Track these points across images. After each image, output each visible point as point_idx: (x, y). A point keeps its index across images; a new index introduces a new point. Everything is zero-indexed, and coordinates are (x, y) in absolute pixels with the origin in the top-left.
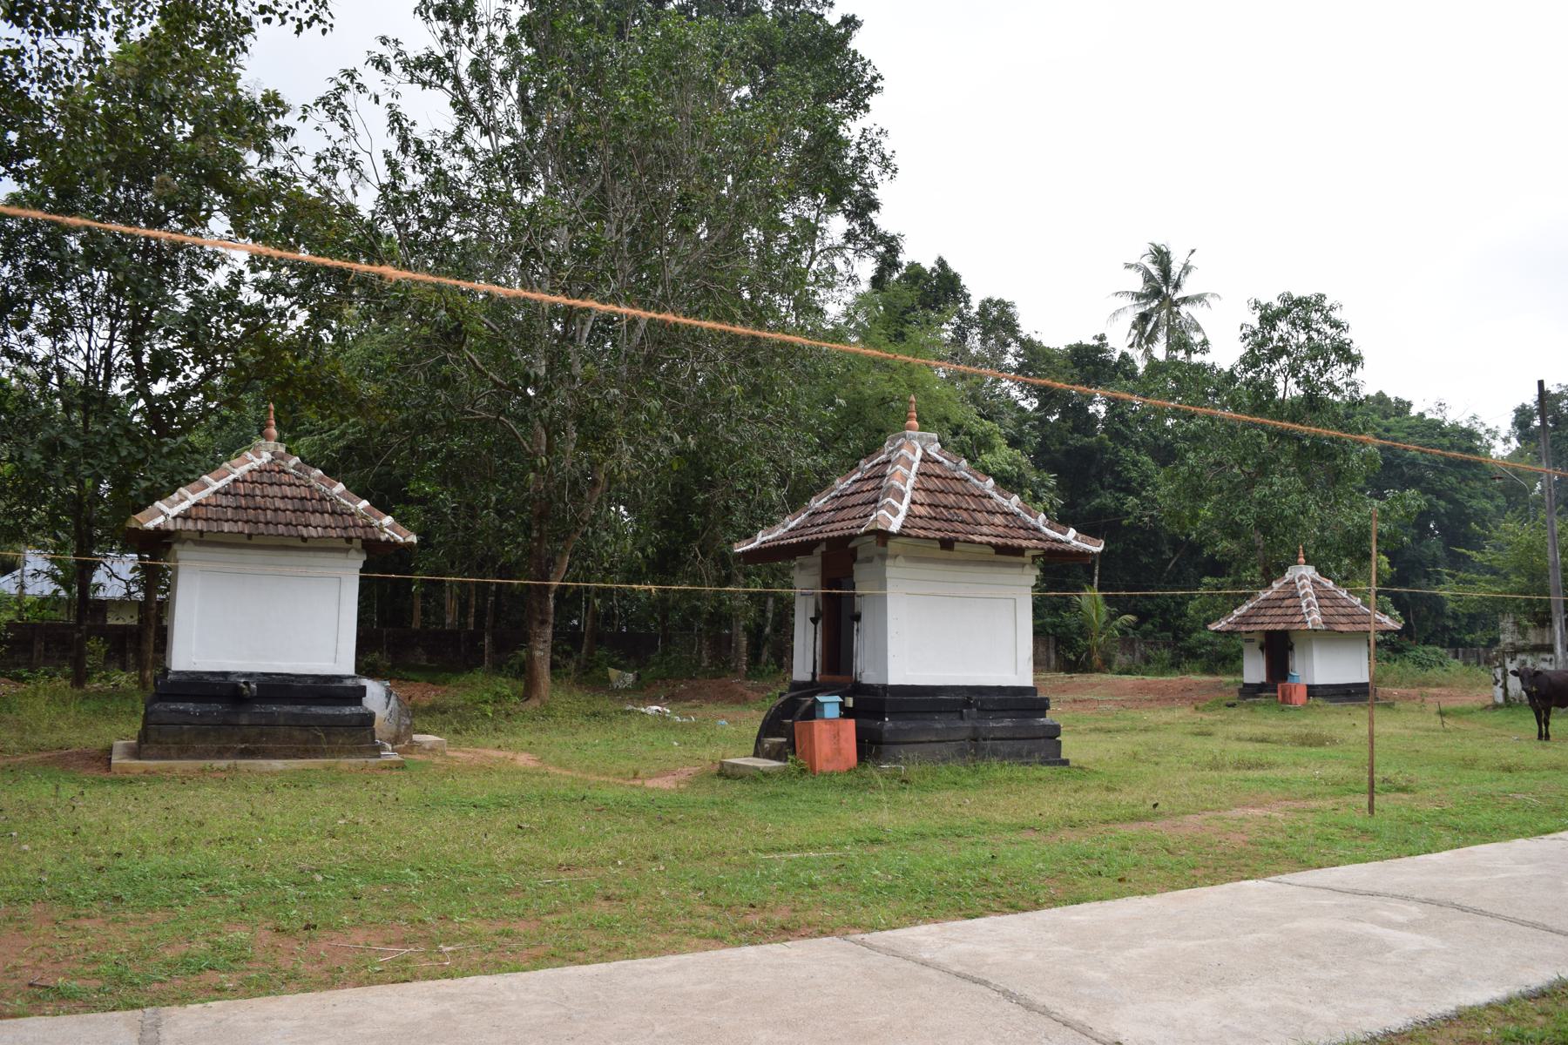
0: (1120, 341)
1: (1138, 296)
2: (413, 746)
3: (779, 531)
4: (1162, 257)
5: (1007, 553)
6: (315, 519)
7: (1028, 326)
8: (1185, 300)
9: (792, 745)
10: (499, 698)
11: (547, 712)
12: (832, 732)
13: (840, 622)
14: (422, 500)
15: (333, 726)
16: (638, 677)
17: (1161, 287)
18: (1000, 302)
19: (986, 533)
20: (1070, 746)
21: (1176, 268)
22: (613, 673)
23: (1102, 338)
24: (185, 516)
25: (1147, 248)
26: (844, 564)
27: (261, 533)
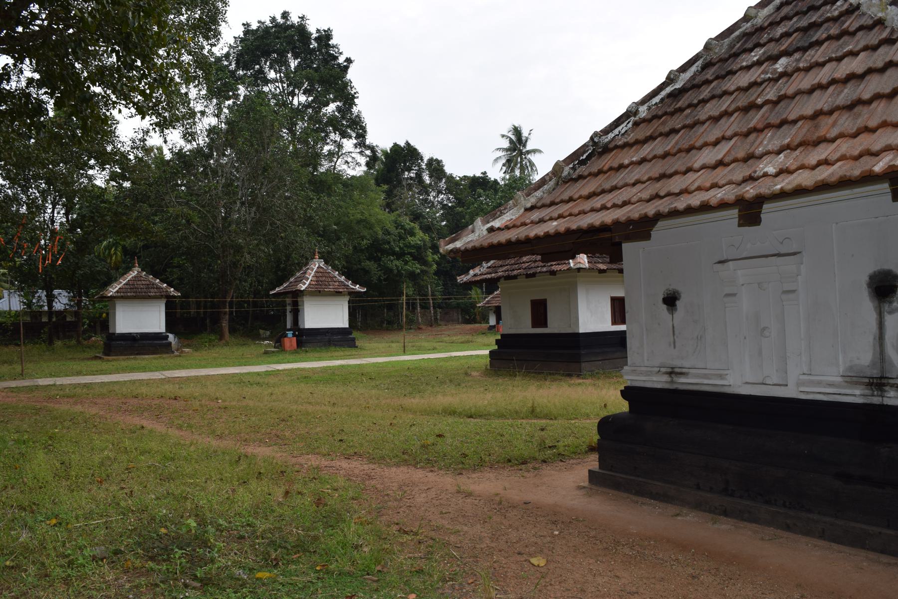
0: (496, 173)
1: (507, 150)
2: (182, 352)
3: (282, 288)
4: (517, 131)
5: (338, 294)
6: (152, 290)
7: (448, 170)
8: (528, 152)
9: (281, 345)
10: (210, 341)
11: (227, 344)
12: (290, 340)
13: (297, 313)
14: (179, 266)
15: (161, 345)
16: (271, 333)
17: (517, 147)
18: (436, 160)
19: (331, 289)
20: (357, 344)
21: (524, 139)
22: (261, 331)
23: (485, 173)
24: (117, 292)
25: (510, 127)
26: (297, 296)
27: (137, 295)
